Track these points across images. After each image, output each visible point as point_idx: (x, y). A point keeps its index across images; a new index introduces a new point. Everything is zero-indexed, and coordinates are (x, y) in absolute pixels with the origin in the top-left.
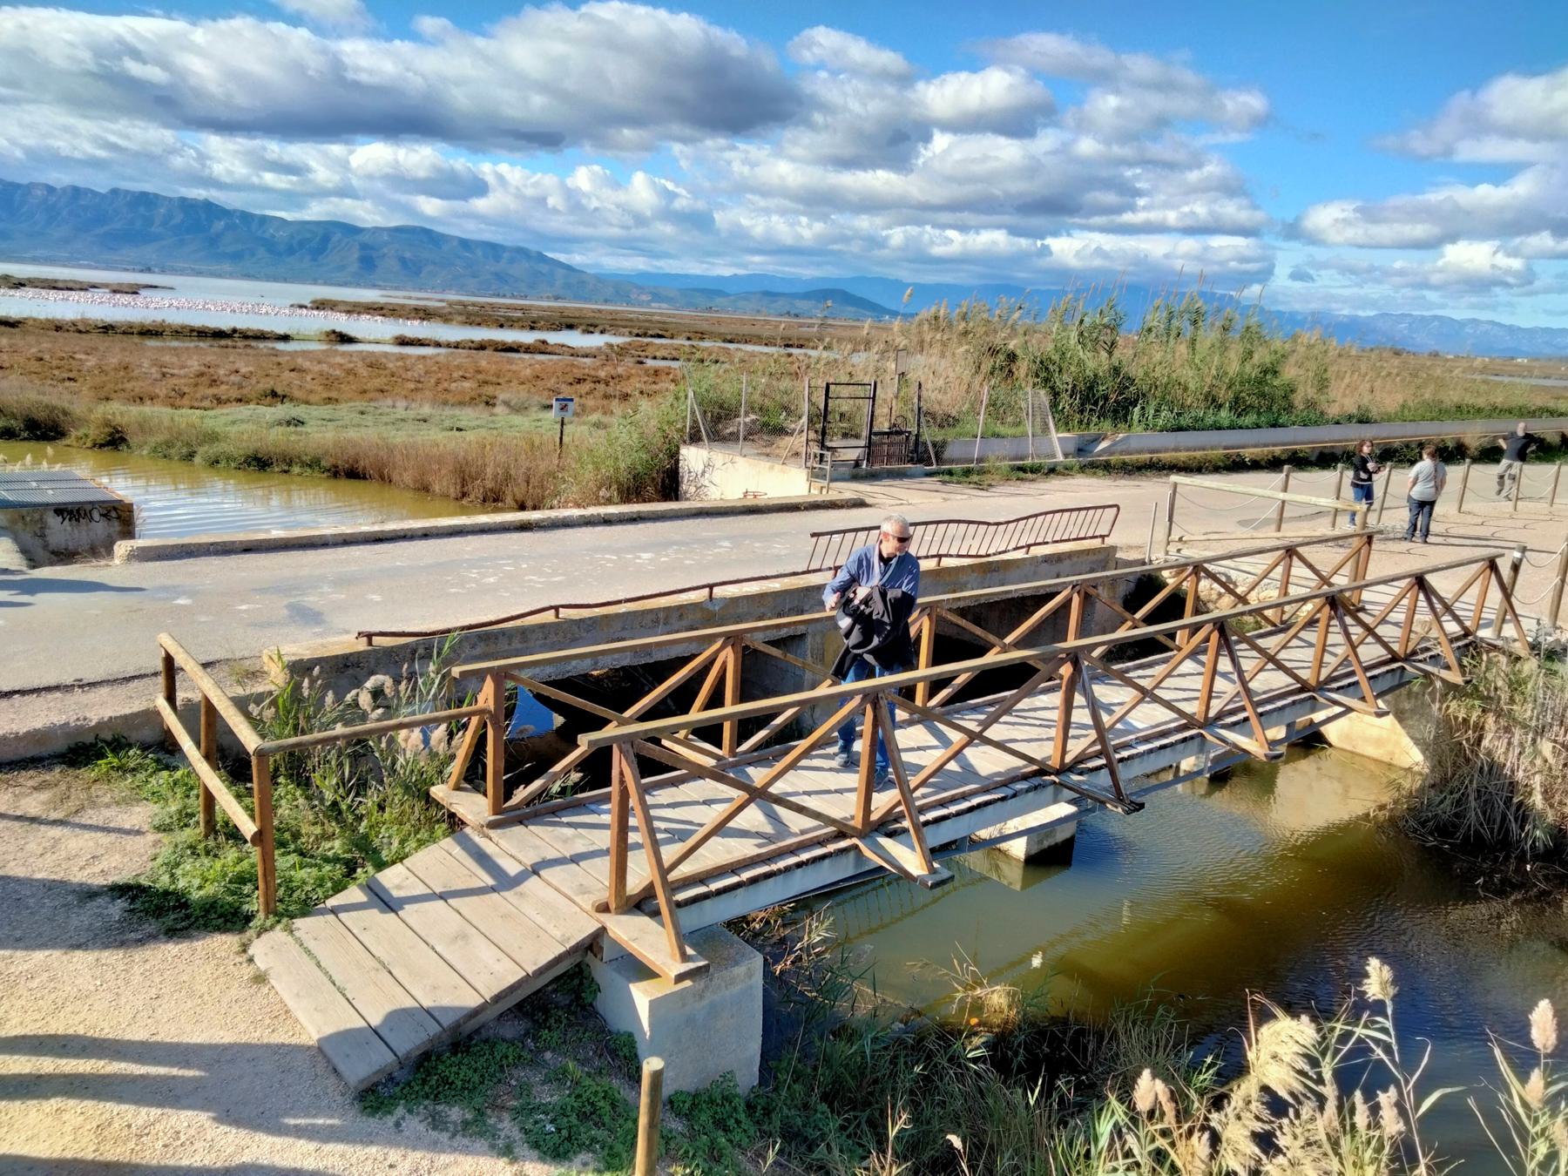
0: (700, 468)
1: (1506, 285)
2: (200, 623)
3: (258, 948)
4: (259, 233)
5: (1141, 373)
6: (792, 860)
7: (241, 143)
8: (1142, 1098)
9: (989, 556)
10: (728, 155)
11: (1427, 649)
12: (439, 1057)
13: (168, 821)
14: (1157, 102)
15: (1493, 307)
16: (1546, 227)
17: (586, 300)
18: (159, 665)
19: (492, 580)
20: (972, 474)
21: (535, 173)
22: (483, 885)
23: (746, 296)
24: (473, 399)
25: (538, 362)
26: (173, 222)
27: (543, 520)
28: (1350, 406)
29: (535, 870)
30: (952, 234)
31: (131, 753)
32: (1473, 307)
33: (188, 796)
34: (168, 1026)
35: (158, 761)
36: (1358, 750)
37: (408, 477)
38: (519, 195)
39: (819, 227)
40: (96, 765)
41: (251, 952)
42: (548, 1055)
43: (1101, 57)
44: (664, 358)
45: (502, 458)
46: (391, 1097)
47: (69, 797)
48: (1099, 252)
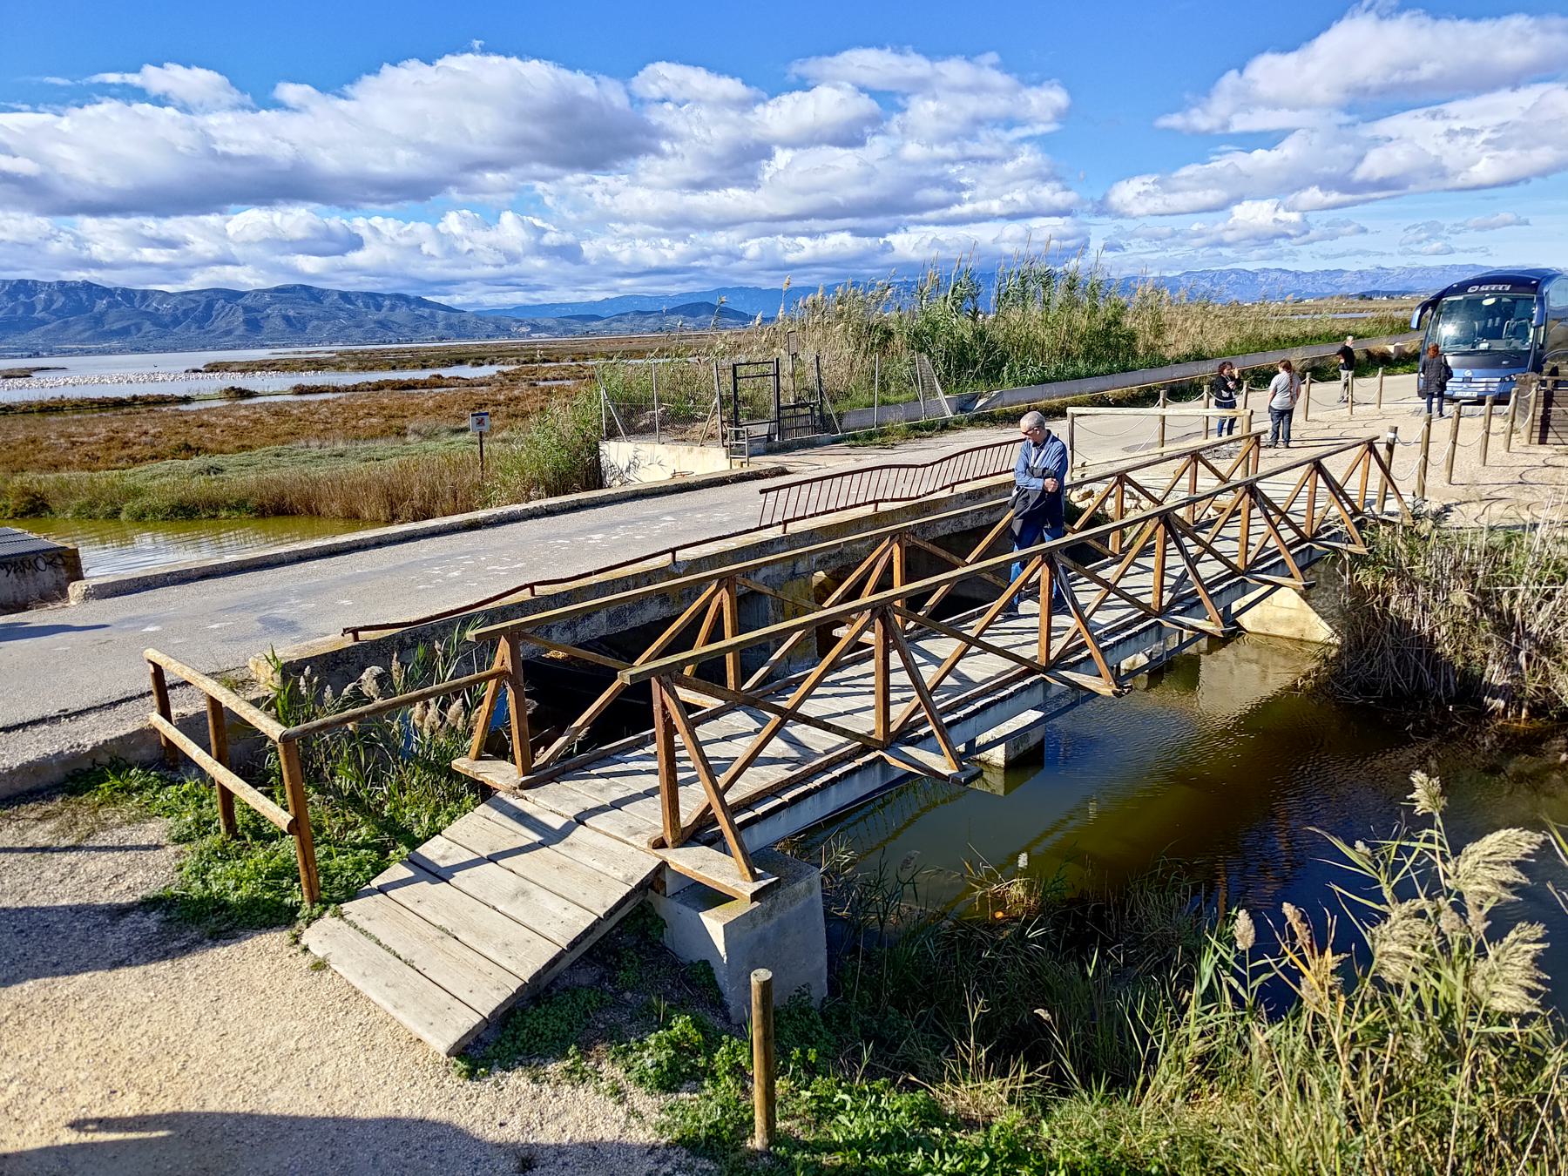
0: (623, 464)
1: (1288, 236)
2: (175, 645)
3: (310, 937)
4: (143, 308)
5: (1001, 337)
6: (826, 778)
7: (116, 223)
8: (1242, 936)
9: (918, 497)
10: (588, 188)
11: (1329, 528)
12: (523, 1012)
13: (186, 832)
14: (972, 105)
15: (1279, 257)
16: (1312, 184)
17: (469, 337)
18: (148, 684)
19: (456, 574)
20: (874, 437)
21: (407, 222)
22: (530, 842)
23: (620, 317)
24: (383, 431)
25: (437, 394)
26: (54, 307)
27: (489, 518)
28: (1184, 348)
29: (580, 820)
30: (802, 240)
31: (132, 773)
32: (1263, 258)
33: (201, 807)
34: (235, 1026)
35: (161, 778)
36: (1271, 632)
37: (335, 506)
38: (394, 245)
39: (680, 247)
40: (99, 789)
41: (304, 942)
42: (628, 995)
43: (917, 66)
44: (555, 379)
45: (427, 477)
46: (483, 1058)
47: (76, 823)
48: (935, 243)
